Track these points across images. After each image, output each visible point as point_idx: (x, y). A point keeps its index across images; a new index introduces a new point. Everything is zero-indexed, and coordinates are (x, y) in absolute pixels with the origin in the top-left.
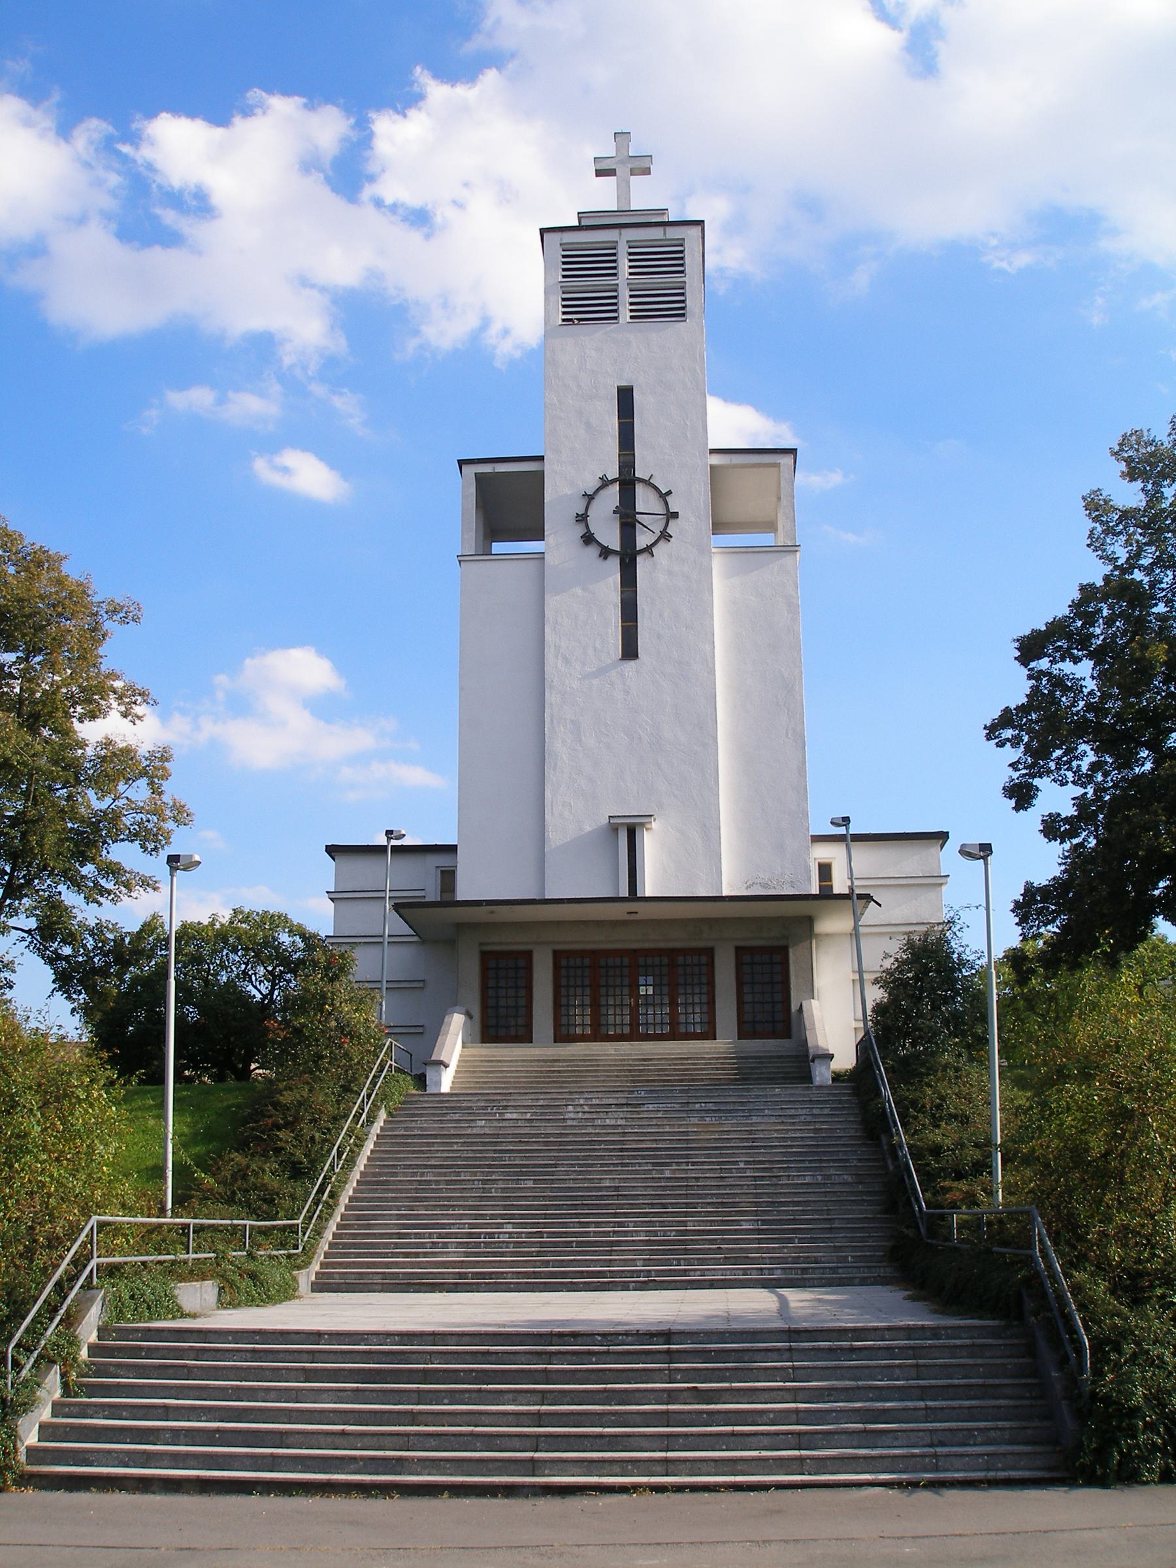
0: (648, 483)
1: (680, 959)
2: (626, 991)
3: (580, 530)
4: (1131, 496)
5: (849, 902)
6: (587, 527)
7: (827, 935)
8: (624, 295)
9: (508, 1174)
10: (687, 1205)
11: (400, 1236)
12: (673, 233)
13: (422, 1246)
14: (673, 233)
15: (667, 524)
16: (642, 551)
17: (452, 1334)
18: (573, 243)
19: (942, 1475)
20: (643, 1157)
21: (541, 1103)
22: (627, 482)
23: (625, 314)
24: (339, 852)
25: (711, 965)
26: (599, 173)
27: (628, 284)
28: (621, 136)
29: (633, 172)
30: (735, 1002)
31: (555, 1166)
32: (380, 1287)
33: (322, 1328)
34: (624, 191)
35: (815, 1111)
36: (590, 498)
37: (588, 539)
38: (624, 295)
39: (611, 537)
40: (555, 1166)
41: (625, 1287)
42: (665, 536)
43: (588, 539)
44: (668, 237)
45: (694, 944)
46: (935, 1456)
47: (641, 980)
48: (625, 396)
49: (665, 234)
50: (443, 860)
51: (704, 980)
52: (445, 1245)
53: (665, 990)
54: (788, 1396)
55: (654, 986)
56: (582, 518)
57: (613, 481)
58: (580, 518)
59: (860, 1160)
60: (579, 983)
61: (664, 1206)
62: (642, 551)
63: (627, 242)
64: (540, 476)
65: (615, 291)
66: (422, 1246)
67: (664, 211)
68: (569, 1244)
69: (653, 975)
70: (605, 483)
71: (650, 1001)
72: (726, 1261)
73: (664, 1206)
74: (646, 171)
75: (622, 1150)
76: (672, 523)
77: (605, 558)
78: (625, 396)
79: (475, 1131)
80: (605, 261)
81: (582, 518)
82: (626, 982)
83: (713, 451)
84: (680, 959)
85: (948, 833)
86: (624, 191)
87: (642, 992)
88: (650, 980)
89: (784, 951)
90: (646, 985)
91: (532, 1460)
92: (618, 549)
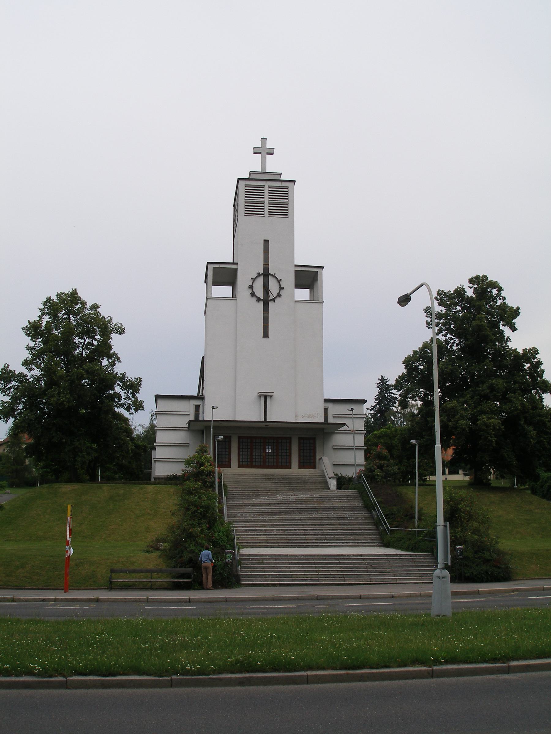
0: (274, 276)
1: (280, 441)
2: (262, 451)
3: (250, 291)
4: (439, 309)
5: (352, 435)
6: (252, 290)
7: (260, 402)
8: (267, 205)
9: (269, 515)
10: (322, 525)
11: (246, 532)
12: (285, 184)
13: (254, 535)
14: (285, 184)
15: (280, 291)
16: (271, 300)
17: (316, 555)
18: (249, 185)
19: (423, 581)
20: (305, 511)
21: (269, 494)
22: (266, 274)
23: (266, 212)
24: (159, 397)
25: (290, 443)
26: (255, 153)
27: (269, 202)
28: (264, 140)
29: (268, 154)
30: (298, 456)
31: (281, 513)
32: (270, 546)
33: (288, 554)
34: (264, 163)
35: (348, 499)
36: (254, 280)
37: (253, 294)
38: (267, 205)
39: (260, 294)
40: (281, 513)
41: (312, 547)
42: (279, 295)
43: (253, 294)
44: (283, 186)
45: (284, 436)
46: (422, 578)
47: (267, 447)
48: (266, 242)
49: (282, 184)
50: (197, 402)
51: (288, 448)
52: (260, 535)
53: (275, 451)
54: (390, 567)
55: (271, 449)
56: (251, 287)
57: (262, 274)
58: (250, 287)
59: (364, 513)
60: (246, 448)
61: (315, 525)
62: (271, 300)
63: (269, 186)
64: (236, 270)
65: (264, 204)
66: (254, 535)
67: (280, 174)
68: (293, 535)
69: (271, 446)
70: (259, 275)
71: (270, 454)
72: (336, 540)
73: (315, 525)
74: (272, 154)
75: (298, 509)
76: (282, 291)
77: (258, 302)
78: (266, 242)
79: (251, 502)
80: (260, 191)
81: (251, 287)
82: (262, 448)
83: (296, 266)
84: (280, 441)
85: (366, 400)
86: (264, 163)
87: (267, 451)
88: (270, 447)
89: (314, 439)
90: (269, 449)
91: (344, 579)
92: (263, 299)
